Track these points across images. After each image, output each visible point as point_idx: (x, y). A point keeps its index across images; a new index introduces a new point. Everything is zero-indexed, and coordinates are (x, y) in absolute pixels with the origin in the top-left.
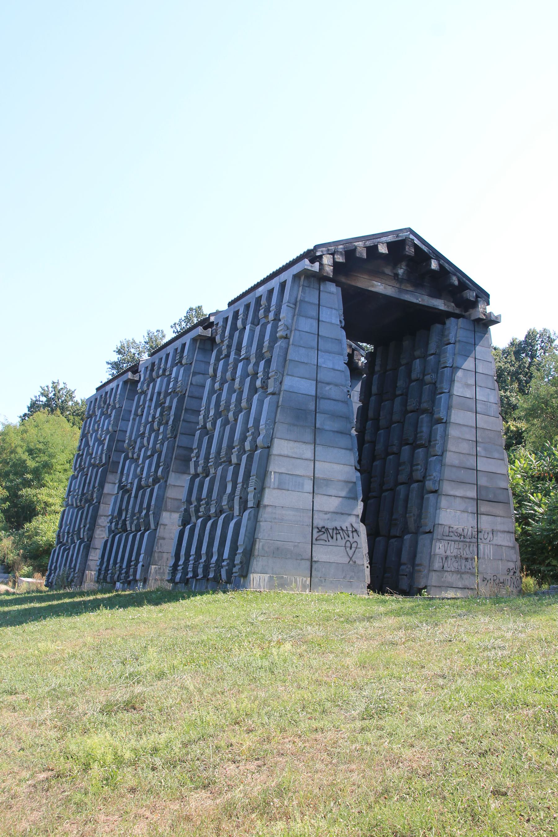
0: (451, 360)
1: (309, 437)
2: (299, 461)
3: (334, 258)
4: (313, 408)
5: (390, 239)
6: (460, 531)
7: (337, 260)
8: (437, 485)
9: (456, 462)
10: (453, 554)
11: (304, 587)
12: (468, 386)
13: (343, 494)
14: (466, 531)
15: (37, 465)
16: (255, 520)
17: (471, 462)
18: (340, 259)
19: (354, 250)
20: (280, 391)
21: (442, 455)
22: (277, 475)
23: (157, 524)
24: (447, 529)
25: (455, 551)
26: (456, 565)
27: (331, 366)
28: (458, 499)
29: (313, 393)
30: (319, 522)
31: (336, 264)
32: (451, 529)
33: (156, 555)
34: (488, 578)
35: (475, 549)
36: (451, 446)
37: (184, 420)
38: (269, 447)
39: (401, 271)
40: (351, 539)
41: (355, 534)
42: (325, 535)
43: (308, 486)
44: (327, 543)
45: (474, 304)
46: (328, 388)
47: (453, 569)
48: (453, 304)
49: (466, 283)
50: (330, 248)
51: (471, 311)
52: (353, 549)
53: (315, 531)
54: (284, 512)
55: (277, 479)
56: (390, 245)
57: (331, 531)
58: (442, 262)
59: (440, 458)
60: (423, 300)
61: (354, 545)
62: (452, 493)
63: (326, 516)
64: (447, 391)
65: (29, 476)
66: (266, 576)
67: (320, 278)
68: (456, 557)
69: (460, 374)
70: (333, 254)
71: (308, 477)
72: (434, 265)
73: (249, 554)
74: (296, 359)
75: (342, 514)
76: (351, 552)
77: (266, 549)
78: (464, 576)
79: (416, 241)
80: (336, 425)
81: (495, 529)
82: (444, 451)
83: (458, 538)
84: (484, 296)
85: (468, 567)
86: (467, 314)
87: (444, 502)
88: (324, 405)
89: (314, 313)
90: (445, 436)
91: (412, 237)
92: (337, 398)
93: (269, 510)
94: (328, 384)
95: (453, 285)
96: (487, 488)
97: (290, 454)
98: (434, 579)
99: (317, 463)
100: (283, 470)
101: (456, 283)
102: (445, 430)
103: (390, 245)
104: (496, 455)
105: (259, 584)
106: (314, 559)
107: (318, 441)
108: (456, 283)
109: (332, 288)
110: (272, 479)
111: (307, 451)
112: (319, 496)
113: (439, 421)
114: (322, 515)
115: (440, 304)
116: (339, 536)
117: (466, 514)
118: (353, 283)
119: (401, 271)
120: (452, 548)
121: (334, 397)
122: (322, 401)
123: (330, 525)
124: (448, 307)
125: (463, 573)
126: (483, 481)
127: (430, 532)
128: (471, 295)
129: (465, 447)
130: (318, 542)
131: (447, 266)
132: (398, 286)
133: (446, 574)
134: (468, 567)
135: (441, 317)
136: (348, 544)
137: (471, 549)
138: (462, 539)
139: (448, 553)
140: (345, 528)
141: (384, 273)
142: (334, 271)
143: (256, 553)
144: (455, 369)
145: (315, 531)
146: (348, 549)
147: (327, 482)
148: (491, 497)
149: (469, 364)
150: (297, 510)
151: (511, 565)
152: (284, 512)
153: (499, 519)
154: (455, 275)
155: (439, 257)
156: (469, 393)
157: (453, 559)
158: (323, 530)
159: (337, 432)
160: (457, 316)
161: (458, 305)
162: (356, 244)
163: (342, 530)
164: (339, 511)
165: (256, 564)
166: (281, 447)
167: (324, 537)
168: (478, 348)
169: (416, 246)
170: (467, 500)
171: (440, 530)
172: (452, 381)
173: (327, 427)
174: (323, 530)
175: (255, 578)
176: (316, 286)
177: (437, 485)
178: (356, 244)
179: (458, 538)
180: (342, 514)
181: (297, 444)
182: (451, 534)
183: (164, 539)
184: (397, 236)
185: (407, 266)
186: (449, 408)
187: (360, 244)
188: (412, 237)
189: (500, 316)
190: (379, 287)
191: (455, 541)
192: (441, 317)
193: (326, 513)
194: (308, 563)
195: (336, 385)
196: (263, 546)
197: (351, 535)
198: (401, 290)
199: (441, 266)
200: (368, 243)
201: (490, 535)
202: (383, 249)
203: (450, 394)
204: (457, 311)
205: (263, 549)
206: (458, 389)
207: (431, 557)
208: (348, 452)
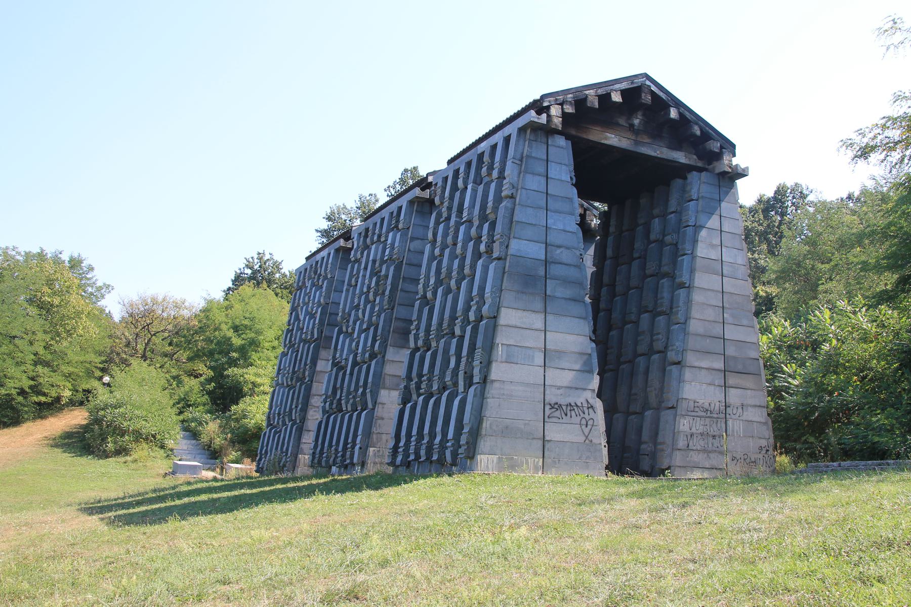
0: (694, 219)
1: (539, 305)
2: (528, 331)
3: (562, 109)
4: (542, 273)
5: (624, 86)
6: (706, 406)
7: (566, 111)
8: (680, 356)
9: (701, 330)
10: (699, 432)
11: (536, 469)
12: (713, 246)
13: (577, 367)
14: (712, 405)
15: (243, 342)
16: (482, 396)
17: (717, 330)
18: (569, 109)
19: (585, 99)
20: (506, 255)
21: (685, 323)
22: (505, 347)
23: (375, 403)
24: (692, 404)
25: (701, 427)
26: (702, 443)
27: (562, 228)
28: (704, 372)
29: (543, 257)
30: (551, 398)
31: (564, 115)
32: (696, 404)
33: (375, 436)
34: (738, 457)
35: (724, 426)
36: (695, 313)
37: (402, 290)
38: (495, 317)
39: (636, 122)
40: (586, 416)
41: (591, 410)
42: (559, 412)
43: (539, 359)
44: (561, 421)
45: (718, 156)
46: (558, 251)
47: (699, 448)
48: (695, 157)
49: (709, 133)
50: (559, 97)
51: (715, 164)
52: (589, 427)
53: (547, 407)
54: (513, 388)
55: (505, 352)
56: (624, 93)
57: (564, 408)
58: (682, 110)
59: (683, 326)
60: (662, 153)
61: (590, 423)
62: (696, 364)
63: (559, 392)
64: (689, 252)
65: (235, 355)
66: (495, 458)
67: (547, 131)
68: (702, 434)
69: (703, 233)
70: (561, 104)
71: (539, 349)
72: (673, 113)
73: (476, 433)
74: (524, 220)
75: (577, 389)
76: (586, 431)
77: (494, 428)
78: (711, 455)
79: (653, 88)
80: (568, 293)
81: (745, 403)
82: (687, 318)
83: (704, 414)
84: (729, 146)
85: (715, 445)
86: (711, 166)
87: (688, 374)
88: (555, 270)
89: (542, 170)
90: (688, 302)
91: (648, 83)
92: (569, 261)
93: (496, 385)
94: (559, 247)
95: (695, 135)
96: (735, 358)
97: (519, 324)
98: (678, 459)
99: (548, 333)
100: (511, 342)
101: (698, 133)
102: (688, 295)
103: (624, 93)
104: (745, 322)
105: (487, 466)
106: (547, 438)
107: (548, 310)
108: (698, 133)
109: (561, 141)
110: (500, 352)
111: (537, 321)
112: (551, 369)
113: (682, 286)
114: (553, 389)
115: (681, 157)
116: (573, 413)
117: (713, 387)
118: (585, 136)
119: (636, 122)
120: (698, 424)
121: (565, 261)
122: (553, 267)
123: (563, 401)
124: (690, 159)
125: (710, 452)
126: (731, 351)
127: (673, 407)
128: (715, 146)
129: (710, 314)
130: (551, 420)
131: (687, 114)
132: (633, 138)
133: (692, 453)
134: (715, 445)
135: (682, 171)
136: (584, 422)
137: (719, 425)
138: (709, 414)
139: (694, 430)
140: (579, 404)
141: (618, 125)
142: (563, 123)
143: (483, 432)
144: (698, 228)
145: (547, 407)
146: (583, 427)
147: (560, 353)
148: (740, 368)
149: (713, 222)
150: (528, 385)
151: (764, 443)
152: (513, 388)
153: (749, 392)
154: (697, 124)
155: (678, 104)
156: (714, 254)
157: (700, 437)
158: (556, 406)
159: (570, 299)
160: (700, 170)
161: (700, 158)
162: (587, 92)
163: (577, 406)
164: (574, 386)
165: (484, 444)
166: (507, 316)
167: (557, 414)
168: (723, 204)
169: (653, 93)
170: (714, 372)
171: (683, 405)
172: (695, 241)
173: (558, 294)
174: (556, 406)
175: (483, 459)
176: (544, 140)
177: (680, 356)
178: (587, 92)
179: (704, 414)
180: (577, 389)
181: (525, 313)
182: (697, 409)
183: (383, 419)
184: (632, 83)
185: (643, 115)
186: (692, 271)
187: (592, 92)
188: (648, 83)
189: (747, 168)
190: (612, 139)
191: (700, 417)
192: (682, 171)
193: (559, 388)
194: (541, 442)
195: (568, 248)
196: (491, 424)
197: (586, 411)
198: (637, 143)
199: (681, 114)
200: (600, 92)
201: (740, 410)
202: (616, 98)
203: (693, 256)
204: (700, 164)
205: (491, 428)
206: (702, 251)
207: (675, 434)
208: (582, 321)
